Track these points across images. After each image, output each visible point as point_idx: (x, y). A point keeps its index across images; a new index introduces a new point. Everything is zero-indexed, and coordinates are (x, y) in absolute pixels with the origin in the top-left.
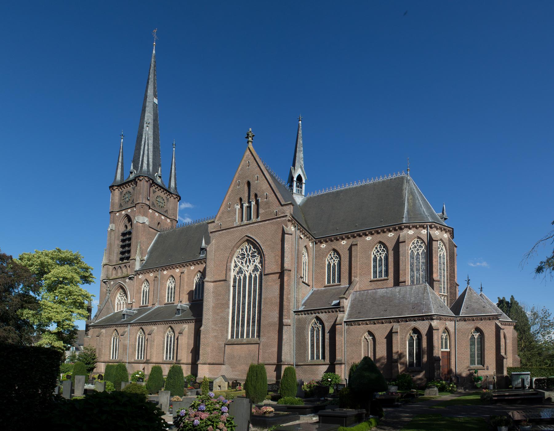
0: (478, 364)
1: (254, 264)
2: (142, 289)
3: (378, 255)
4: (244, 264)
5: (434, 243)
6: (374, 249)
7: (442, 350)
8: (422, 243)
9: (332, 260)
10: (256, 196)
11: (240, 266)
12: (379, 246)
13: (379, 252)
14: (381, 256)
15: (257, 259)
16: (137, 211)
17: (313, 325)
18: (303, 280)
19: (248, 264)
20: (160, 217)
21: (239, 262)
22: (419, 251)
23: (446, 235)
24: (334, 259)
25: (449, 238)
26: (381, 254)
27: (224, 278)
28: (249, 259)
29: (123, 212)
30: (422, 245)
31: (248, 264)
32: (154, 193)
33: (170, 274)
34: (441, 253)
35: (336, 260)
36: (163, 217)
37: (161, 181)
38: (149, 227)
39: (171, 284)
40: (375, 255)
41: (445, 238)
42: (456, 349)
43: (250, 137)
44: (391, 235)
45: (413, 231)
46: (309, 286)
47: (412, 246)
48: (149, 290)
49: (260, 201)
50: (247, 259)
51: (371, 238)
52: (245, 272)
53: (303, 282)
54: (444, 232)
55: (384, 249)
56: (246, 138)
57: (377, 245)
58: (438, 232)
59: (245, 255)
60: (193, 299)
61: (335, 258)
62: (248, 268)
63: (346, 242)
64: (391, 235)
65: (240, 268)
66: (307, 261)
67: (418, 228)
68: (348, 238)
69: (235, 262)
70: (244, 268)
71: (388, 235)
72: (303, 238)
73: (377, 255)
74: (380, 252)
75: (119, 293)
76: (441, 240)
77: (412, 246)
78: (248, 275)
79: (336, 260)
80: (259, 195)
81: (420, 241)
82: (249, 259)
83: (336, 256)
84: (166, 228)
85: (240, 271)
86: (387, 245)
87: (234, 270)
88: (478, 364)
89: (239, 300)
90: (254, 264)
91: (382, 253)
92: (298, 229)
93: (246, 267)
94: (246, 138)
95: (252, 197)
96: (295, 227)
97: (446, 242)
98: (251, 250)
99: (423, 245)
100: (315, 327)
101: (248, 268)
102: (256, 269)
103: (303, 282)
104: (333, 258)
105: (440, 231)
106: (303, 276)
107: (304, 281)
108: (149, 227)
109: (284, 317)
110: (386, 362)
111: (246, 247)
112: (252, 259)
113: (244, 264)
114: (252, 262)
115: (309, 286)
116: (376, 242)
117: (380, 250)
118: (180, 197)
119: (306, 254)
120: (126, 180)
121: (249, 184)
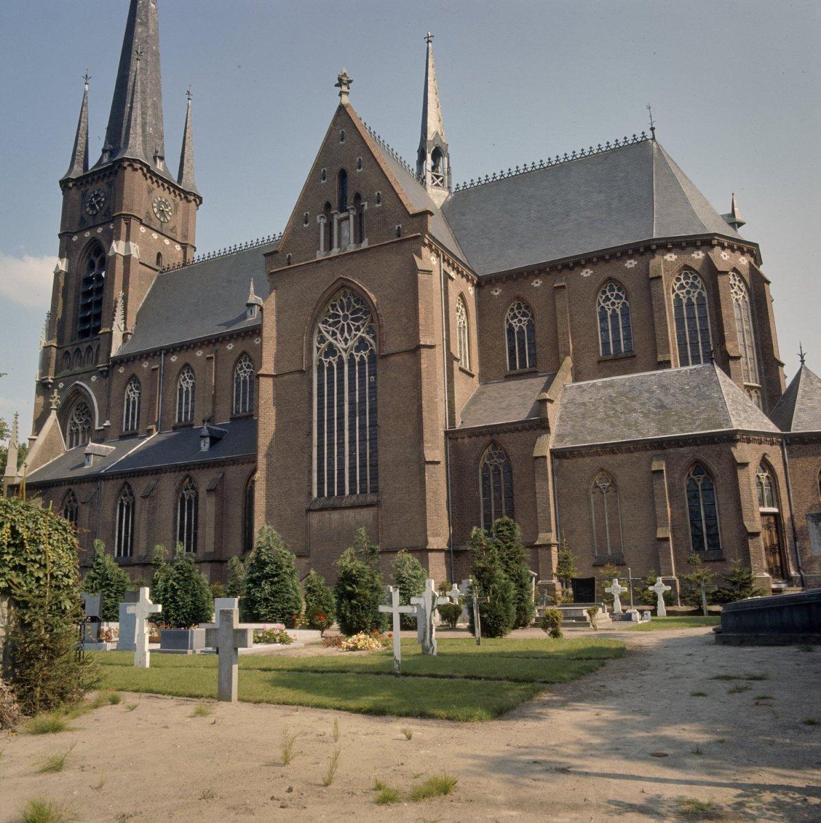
1: (359, 334)
2: (126, 397)
4: (339, 336)
5: (721, 279)
6: (600, 294)
7: (763, 510)
8: (695, 278)
10: (358, 197)
11: (331, 339)
12: (516, 305)
13: (517, 317)
15: (363, 325)
16: (115, 231)
17: (486, 461)
18: (461, 364)
19: (346, 334)
20: (162, 241)
21: (328, 332)
22: (616, 305)
23: (744, 258)
25: (750, 263)
26: (613, 304)
28: (348, 324)
29: (87, 234)
31: (346, 334)
32: (149, 193)
33: (183, 362)
34: (738, 297)
36: (167, 242)
37: (165, 166)
38: (141, 263)
41: (742, 266)
42: (793, 508)
43: (345, 84)
44: (631, 263)
46: (472, 376)
47: (677, 286)
48: (193, 387)
49: (366, 207)
50: (343, 325)
51: (592, 272)
52: (340, 352)
53: (461, 369)
54: (738, 253)
56: (336, 85)
57: (605, 286)
58: (726, 254)
59: (339, 316)
60: (232, 414)
61: (615, 298)
62: (346, 344)
64: (587, 272)
65: (331, 345)
67: (685, 247)
69: (320, 332)
70: (338, 345)
71: (626, 265)
72: (454, 277)
74: (613, 300)
75: (74, 408)
76: (735, 270)
77: (677, 286)
78: (345, 356)
79: (525, 321)
80: (363, 197)
81: (692, 274)
82: (348, 324)
84: (174, 264)
85: (331, 351)
86: (626, 284)
87: (318, 349)
89: (331, 464)
90: (359, 334)
91: (616, 301)
92: (444, 260)
93: (342, 342)
94: (336, 85)
95: (350, 200)
96: (438, 256)
97: (745, 273)
98: (352, 307)
99: (699, 282)
100: (491, 465)
101: (346, 344)
102: (362, 344)
103: (461, 369)
104: (610, 299)
105: (729, 251)
106: (458, 356)
107: (463, 366)
108: (141, 263)
109: (426, 445)
111: (341, 300)
112: (354, 325)
113: (339, 336)
114: (354, 332)
115: (472, 376)
116: (602, 280)
117: (519, 313)
118: (201, 198)
119: (464, 310)
120: (94, 167)
121: (343, 175)
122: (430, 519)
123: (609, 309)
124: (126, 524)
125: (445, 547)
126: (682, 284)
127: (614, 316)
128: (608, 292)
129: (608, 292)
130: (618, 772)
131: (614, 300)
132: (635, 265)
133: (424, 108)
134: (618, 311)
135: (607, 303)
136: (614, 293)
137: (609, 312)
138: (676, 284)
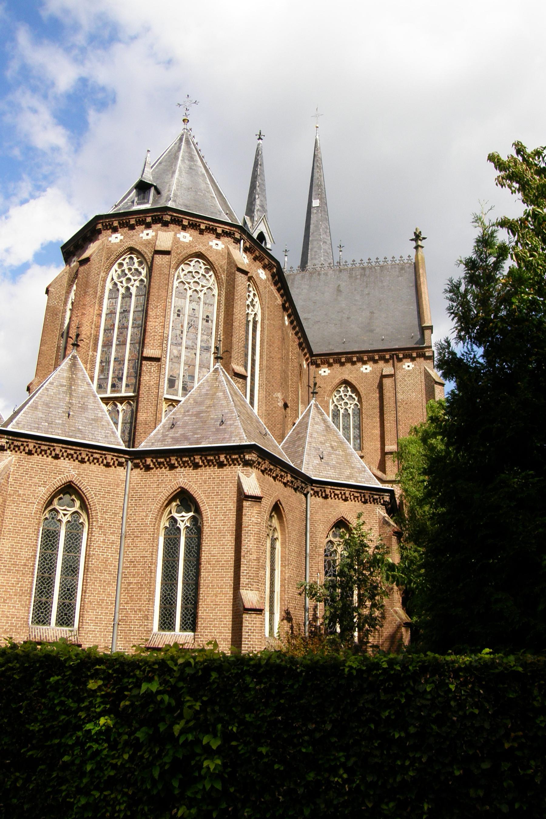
0: (184, 628)
3: (341, 405)
9: (342, 403)
14: (347, 407)
22: (349, 406)
24: (129, 276)
26: (346, 403)
27: (157, 256)
30: (140, 269)
35: (135, 280)
39: (124, 279)
40: (115, 284)
45: (223, 243)
55: (354, 395)
63: (371, 369)
66: (259, 318)
68: (375, 362)
73: (119, 284)
74: (346, 400)
79: (135, 280)
83: (350, 396)
88: (184, 628)
91: (132, 278)
110: (153, 773)
116: (337, 381)
117: (346, 395)
118: (98, 218)
122: (228, 641)
123: (342, 408)
124: (175, 568)
125: (245, 650)
126: (341, 396)
127: (347, 415)
128: (342, 392)
129: (342, 392)
130: (377, 432)
131: (347, 401)
132: (121, 240)
133: (307, 217)
134: (350, 411)
135: (341, 402)
136: (348, 394)
137: (342, 411)
138: (335, 396)
